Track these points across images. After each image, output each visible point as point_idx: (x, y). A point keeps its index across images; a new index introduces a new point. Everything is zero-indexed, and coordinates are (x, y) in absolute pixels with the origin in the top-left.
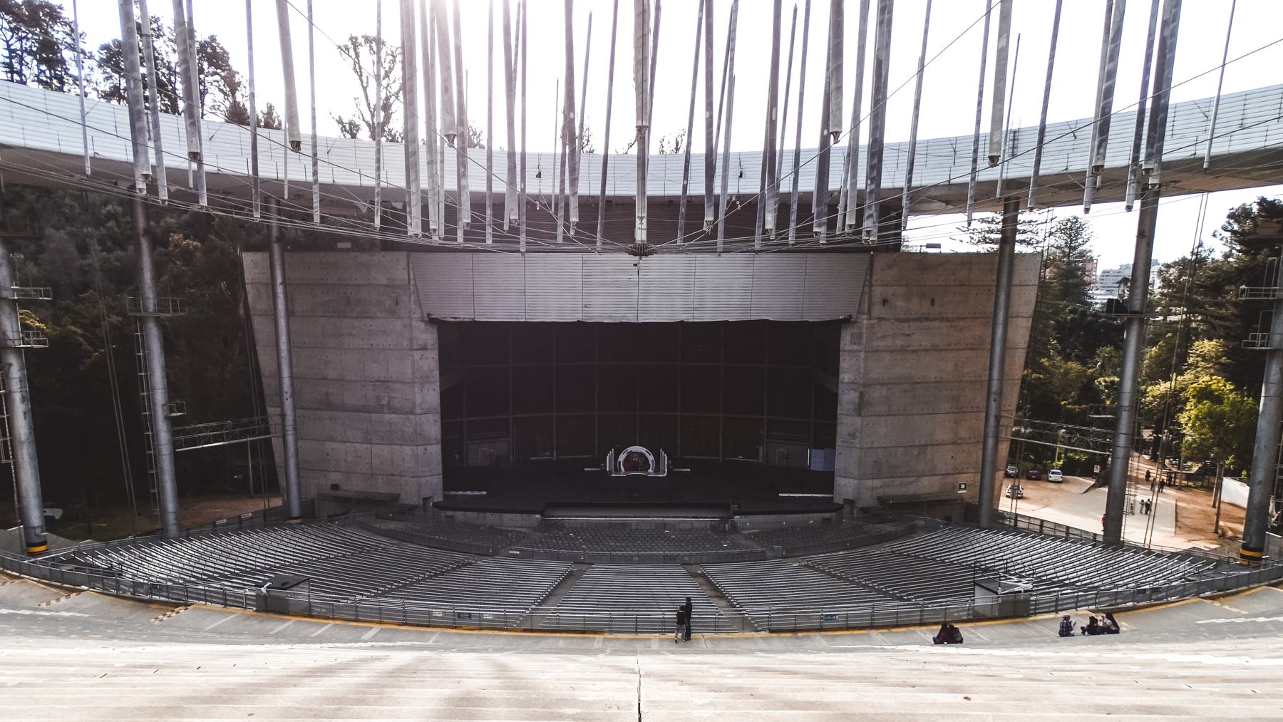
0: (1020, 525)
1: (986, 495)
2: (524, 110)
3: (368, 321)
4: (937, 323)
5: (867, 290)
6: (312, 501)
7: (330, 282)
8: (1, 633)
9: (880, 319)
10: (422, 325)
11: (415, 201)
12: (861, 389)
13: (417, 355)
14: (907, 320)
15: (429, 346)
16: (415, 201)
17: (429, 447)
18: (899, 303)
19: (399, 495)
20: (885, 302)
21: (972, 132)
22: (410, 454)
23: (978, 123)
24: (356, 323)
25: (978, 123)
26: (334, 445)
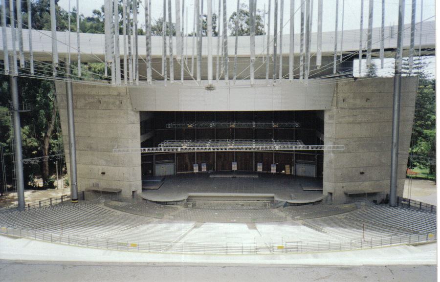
0: (411, 204)
1: (393, 189)
2: (187, 11)
3: (108, 111)
4: (369, 110)
5: (335, 95)
6: (83, 192)
7: (92, 94)
8: (176, 1)
9: (342, 108)
10: (132, 113)
11: (164, 59)
12: (334, 140)
13: (130, 126)
14: (355, 109)
15: (135, 122)
16: (164, 59)
17: (135, 168)
18: (351, 101)
19: (120, 192)
20: (344, 100)
21: (359, 28)
22: (128, 171)
23: (337, 26)
24: (103, 112)
25: (337, 26)
26: (93, 166)
